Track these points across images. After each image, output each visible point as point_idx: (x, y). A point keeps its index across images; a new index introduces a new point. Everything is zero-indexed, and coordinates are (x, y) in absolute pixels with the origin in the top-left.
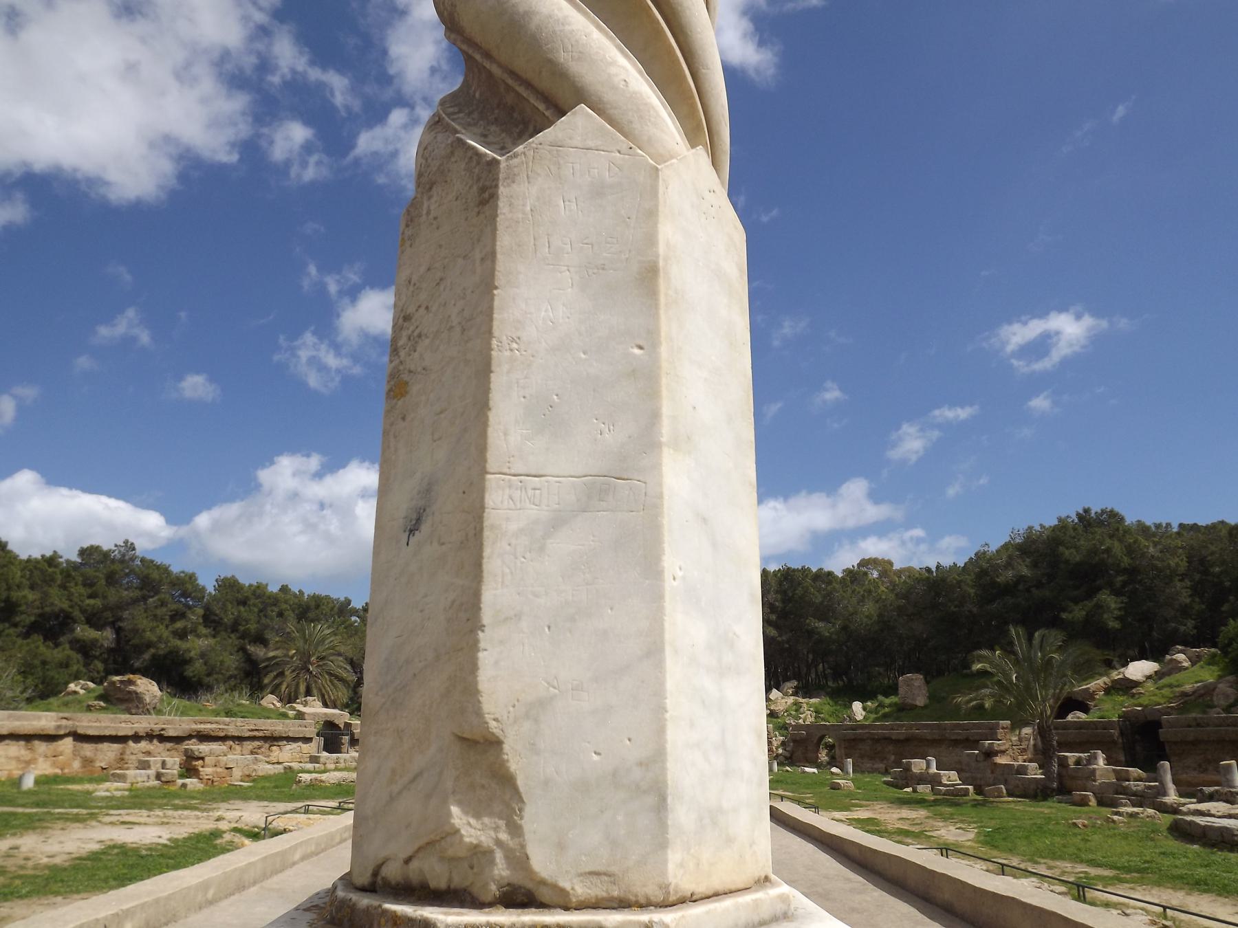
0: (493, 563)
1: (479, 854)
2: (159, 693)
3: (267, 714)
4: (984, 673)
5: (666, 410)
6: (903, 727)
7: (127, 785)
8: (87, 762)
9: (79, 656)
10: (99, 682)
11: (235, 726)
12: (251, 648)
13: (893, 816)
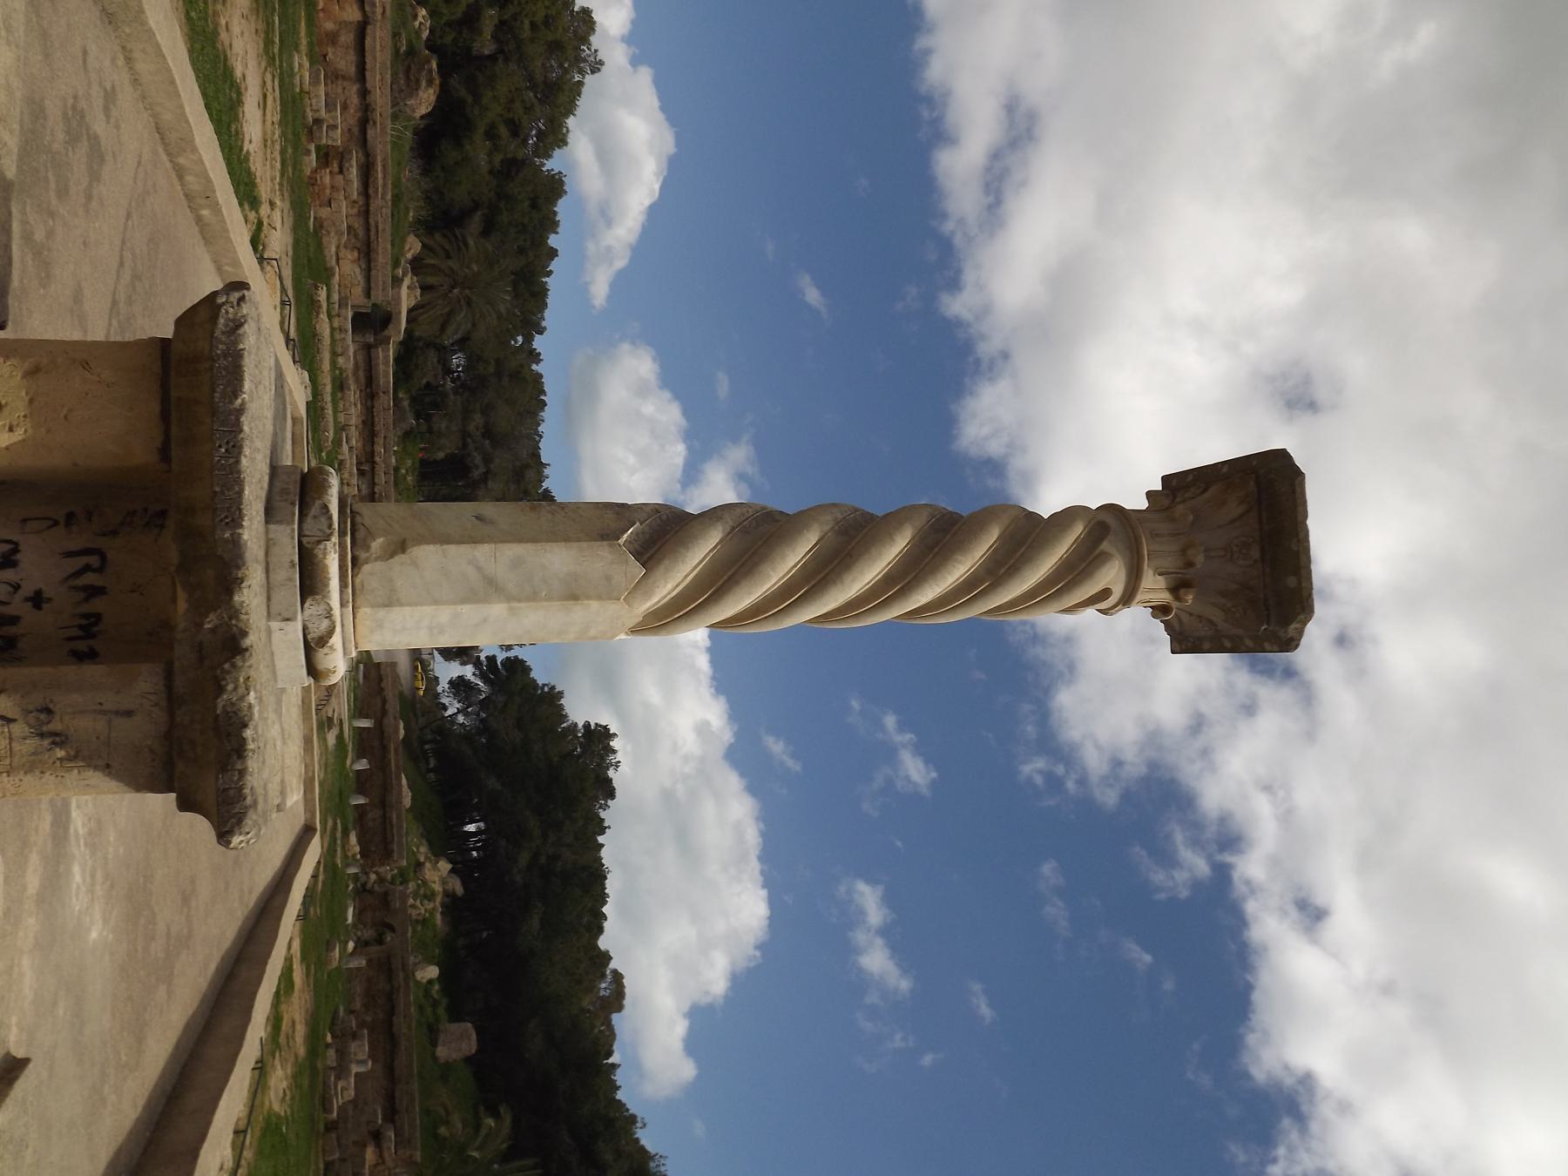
0: (463, 548)
1: (368, 548)
2: (417, 115)
3: (398, 242)
5: (522, 605)
7: (306, 87)
8: (333, 38)
9: (459, 15)
10: (431, 46)
12: (477, 218)
13: (297, 1011)
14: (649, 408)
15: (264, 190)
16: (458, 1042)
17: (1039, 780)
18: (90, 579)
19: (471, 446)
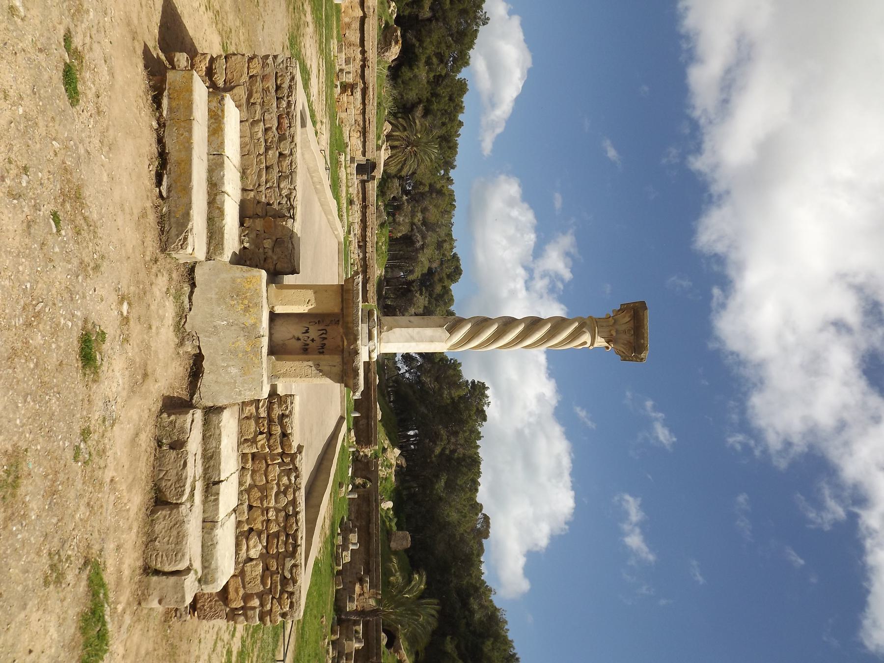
3: (379, 126)
4: (410, 580)
6: (376, 531)
8: (348, 25)
10: (398, 20)
11: (372, 109)
12: (421, 107)
14: (515, 213)
15: (318, 118)
16: (402, 540)
17: (738, 447)
18: (324, 336)
19: (416, 230)
